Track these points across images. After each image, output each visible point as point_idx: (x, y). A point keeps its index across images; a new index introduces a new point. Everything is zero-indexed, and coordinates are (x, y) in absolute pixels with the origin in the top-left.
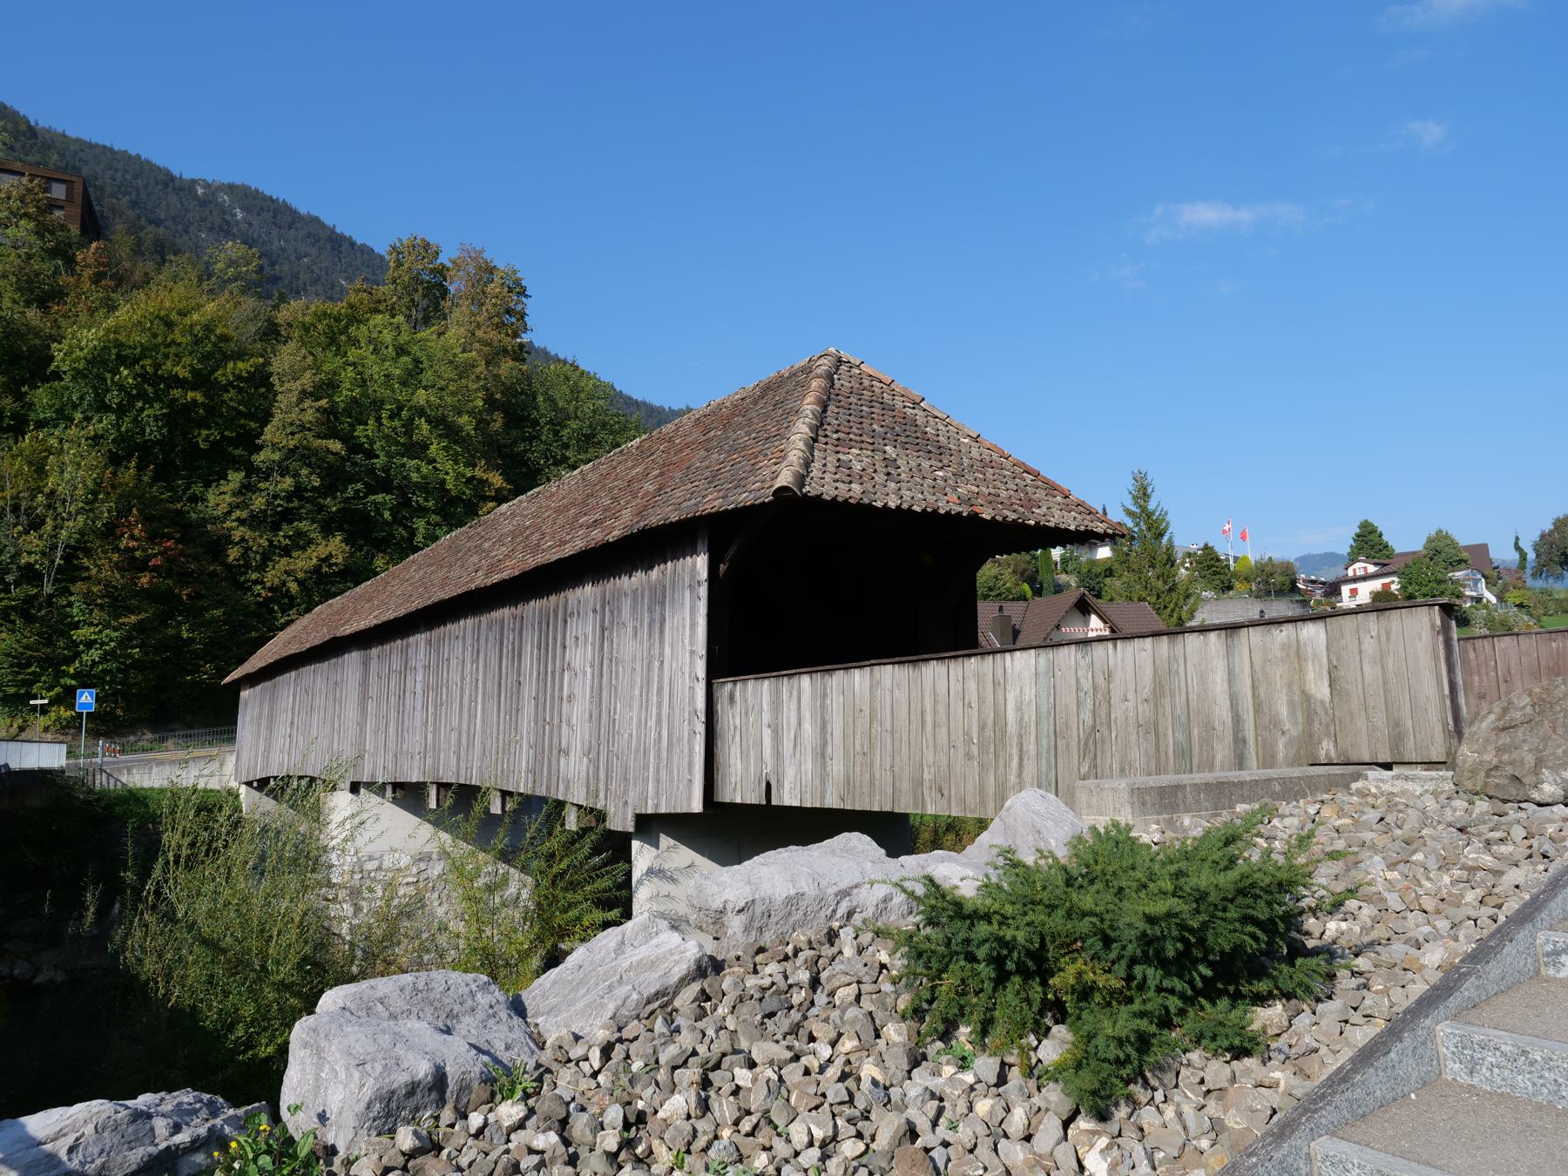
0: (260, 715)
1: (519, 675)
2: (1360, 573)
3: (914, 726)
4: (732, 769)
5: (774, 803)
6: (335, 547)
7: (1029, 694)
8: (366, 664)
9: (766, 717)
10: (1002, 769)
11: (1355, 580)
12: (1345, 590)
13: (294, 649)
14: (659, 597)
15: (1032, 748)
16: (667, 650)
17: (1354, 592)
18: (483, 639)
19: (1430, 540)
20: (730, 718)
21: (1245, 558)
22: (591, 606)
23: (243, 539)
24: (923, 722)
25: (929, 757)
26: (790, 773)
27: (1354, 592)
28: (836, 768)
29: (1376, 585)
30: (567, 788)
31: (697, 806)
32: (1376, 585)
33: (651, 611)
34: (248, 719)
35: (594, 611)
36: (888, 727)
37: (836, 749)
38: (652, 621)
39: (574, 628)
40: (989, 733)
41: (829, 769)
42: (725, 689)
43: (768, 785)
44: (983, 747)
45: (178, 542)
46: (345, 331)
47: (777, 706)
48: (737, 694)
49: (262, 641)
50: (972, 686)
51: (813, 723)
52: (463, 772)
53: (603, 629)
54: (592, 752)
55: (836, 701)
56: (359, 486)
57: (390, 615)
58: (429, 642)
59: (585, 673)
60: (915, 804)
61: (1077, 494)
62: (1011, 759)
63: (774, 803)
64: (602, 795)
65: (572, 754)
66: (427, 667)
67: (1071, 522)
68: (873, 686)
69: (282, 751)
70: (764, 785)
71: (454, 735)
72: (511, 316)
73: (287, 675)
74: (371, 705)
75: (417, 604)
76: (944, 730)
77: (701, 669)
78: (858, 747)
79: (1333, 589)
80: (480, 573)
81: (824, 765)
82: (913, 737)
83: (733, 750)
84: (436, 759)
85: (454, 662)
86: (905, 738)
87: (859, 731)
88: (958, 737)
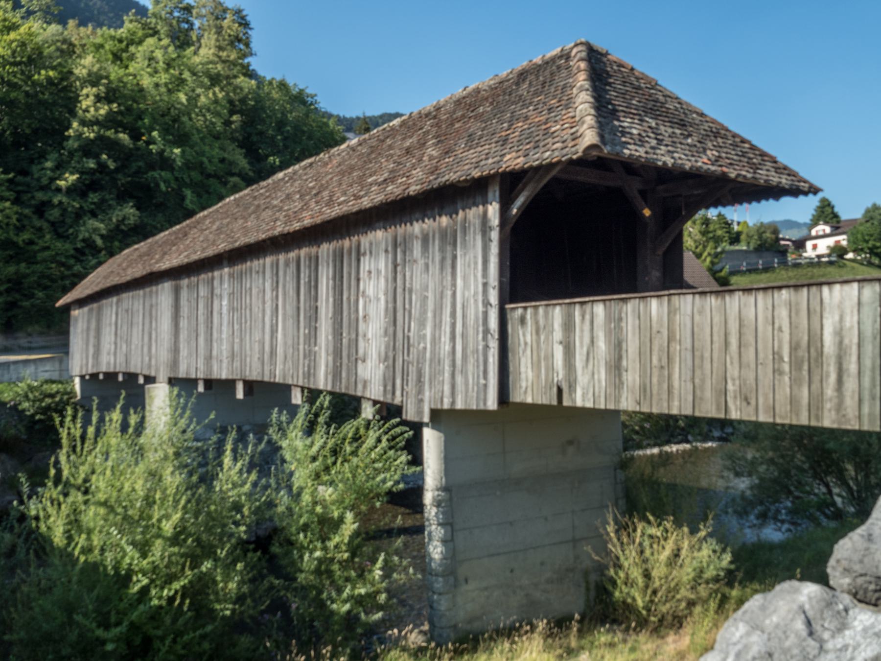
0: (88, 329)
1: (316, 300)
2: (821, 233)
3: (716, 346)
4: (523, 376)
5: (566, 403)
6: (129, 212)
7: (851, 320)
8: (177, 291)
9: (558, 335)
10: (815, 386)
11: (818, 237)
12: (809, 244)
13: (116, 280)
14: (449, 239)
15: (852, 367)
16: (459, 282)
17: (815, 247)
18: (281, 273)
19: (868, 211)
20: (523, 337)
21: (745, 222)
22: (383, 246)
23: (60, 203)
24: (727, 344)
25: (733, 371)
26: (582, 379)
27: (815, 247)
28: (632, 377)
29: (831, 241)
30: (365, 387)
31: (492, 403)
32: (831, 241)
33: (442, 250)
34: (79, 330)
35: (386, 251)
36: (689, 346)
37: (631, 360)
38: (443, 260)
39: (366, 264)
40: (802, 353)
41: (624, 378)
42: (516, 311)
43: (560, 391)
44: (796, 364)
45: (13, 203)
46: (126, 50)
47: (568, 326)
48: (528, 316)
49: (81, 277)
50: (783, 314)
51: (608, 341)
52: (267, 372)
53: (395, 266)
54: (390, 359)
55: (630, 324)
56: (141, 164)
57: (195, 257)
58: (231, 276)
59: (378, 300)
60: (718, 409)
61: (783, 159)
62: (828, 376)
63: (566, 403)
64: (398, 393)
65: (369, 361)
66: (231, 294)
67: (785, 181)
68: (671, 313)
69: (109, 354)
70: (555, 389)
71: (256, 347)
72: (240, 42)
73: (110, 300)
74: (183, 323)
75: (223, 246)
76: (752, 350)
77: (494, 297)
78: (655, 361)
79: (800, 245)
80: (279, 223)
81: (620, 376)
82: (715, 356)
83: (523, 361)
84: (243, 361)
85: (254, 291)
86: (707, 355)
87: (656, 348)
88: (766, 355)
